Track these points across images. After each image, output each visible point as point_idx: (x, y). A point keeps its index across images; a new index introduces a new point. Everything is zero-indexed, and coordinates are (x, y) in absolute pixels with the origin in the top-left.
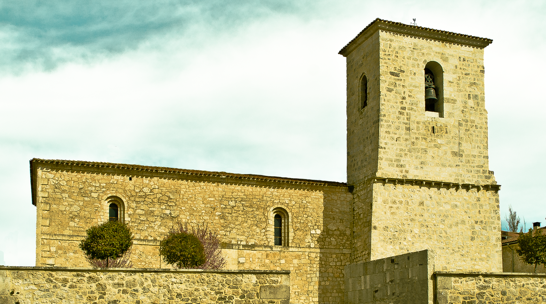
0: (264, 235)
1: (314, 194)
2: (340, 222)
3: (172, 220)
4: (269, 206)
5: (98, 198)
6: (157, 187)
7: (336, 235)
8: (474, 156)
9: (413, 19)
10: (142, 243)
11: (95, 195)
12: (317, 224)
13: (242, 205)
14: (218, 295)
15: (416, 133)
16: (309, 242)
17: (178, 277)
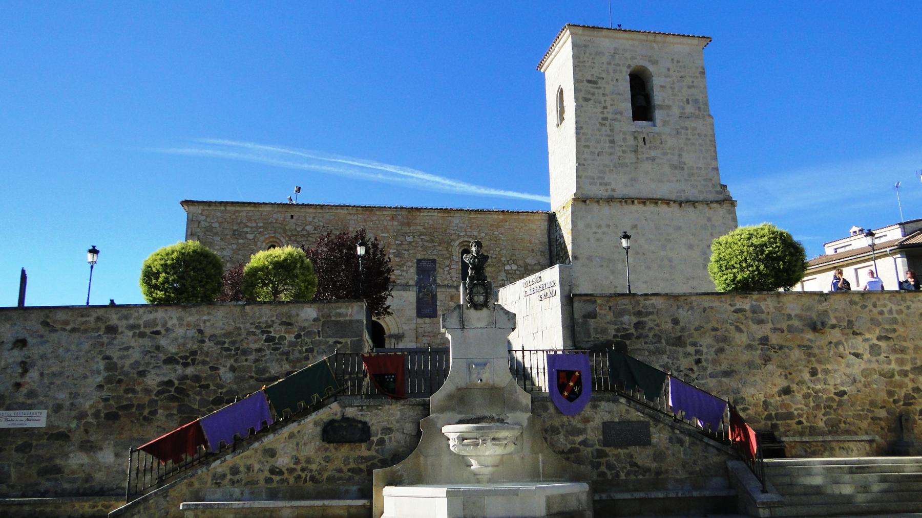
4: (453, 240)
5: (254, 239)
11: (250, 236)
12: (513, 258)
14: (265, 335)
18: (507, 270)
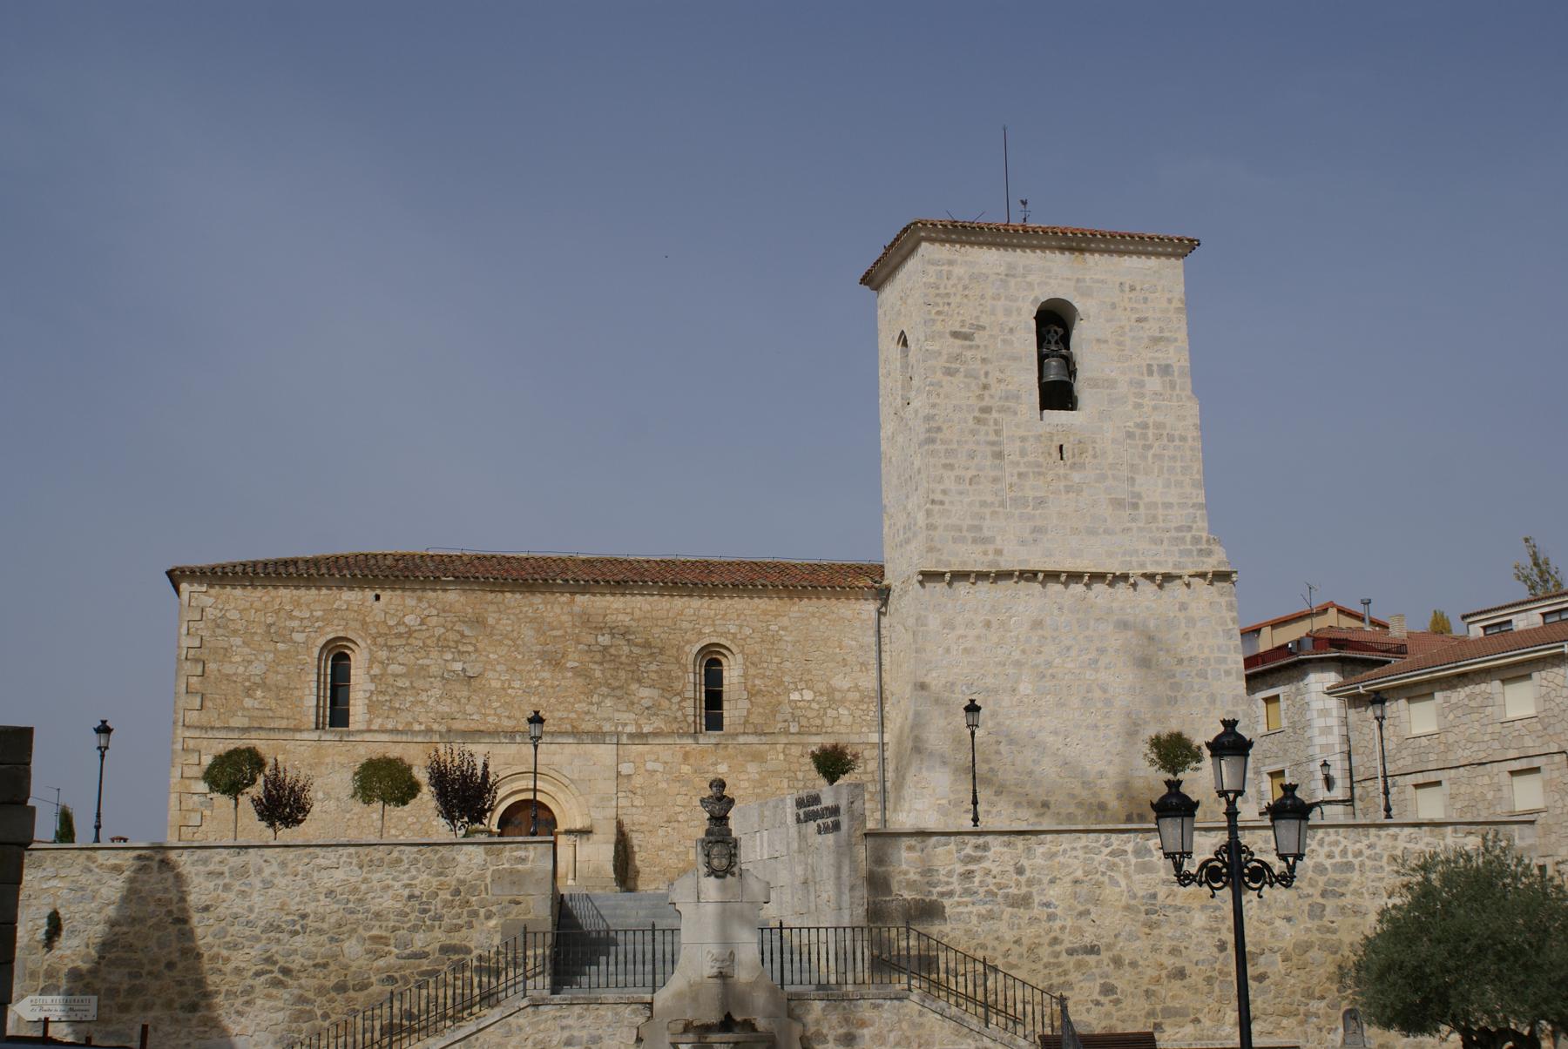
0: (678, 710)
1: (796, 608)
2: (861, 671)
3: (469, 684)
4: (688, 642)
6: (435, 612)
7: (851, 701)
8: (1168, 506)
9: (1022, 202)
10: (398, 738)
11: (298, 637)
13: (626, 643)
15: (1018, 464)
16: (785, 721)
17: (332, 855)
18: (795, 701)
